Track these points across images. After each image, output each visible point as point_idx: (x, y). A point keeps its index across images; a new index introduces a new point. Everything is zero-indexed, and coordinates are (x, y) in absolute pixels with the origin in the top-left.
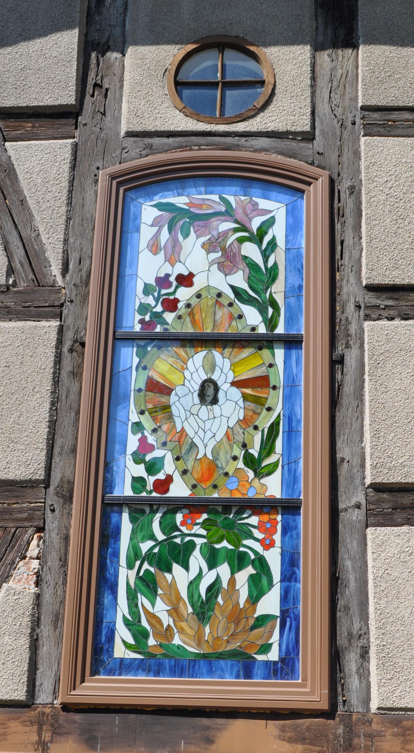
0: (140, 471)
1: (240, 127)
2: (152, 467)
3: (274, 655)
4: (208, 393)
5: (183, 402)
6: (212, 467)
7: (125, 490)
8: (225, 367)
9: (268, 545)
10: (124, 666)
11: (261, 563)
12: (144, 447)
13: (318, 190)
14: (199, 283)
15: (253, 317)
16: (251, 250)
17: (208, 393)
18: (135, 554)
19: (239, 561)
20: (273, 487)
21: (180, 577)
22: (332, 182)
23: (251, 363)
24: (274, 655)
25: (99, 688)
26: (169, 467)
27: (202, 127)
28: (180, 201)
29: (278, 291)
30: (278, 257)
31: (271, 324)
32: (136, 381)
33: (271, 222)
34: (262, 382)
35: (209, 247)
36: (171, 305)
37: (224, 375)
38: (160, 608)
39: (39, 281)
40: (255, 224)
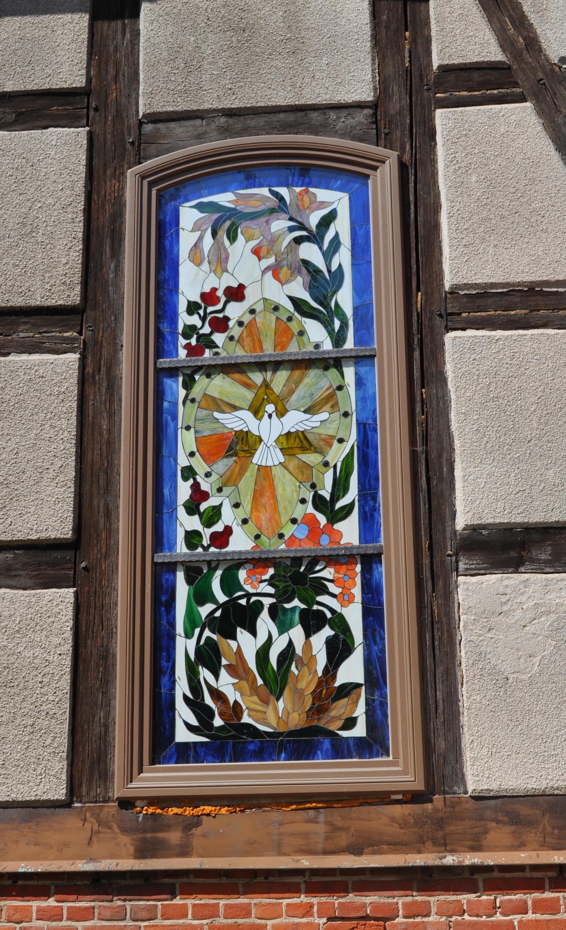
11: (339, 623)
19: (312, 622)
38: (225, 683)
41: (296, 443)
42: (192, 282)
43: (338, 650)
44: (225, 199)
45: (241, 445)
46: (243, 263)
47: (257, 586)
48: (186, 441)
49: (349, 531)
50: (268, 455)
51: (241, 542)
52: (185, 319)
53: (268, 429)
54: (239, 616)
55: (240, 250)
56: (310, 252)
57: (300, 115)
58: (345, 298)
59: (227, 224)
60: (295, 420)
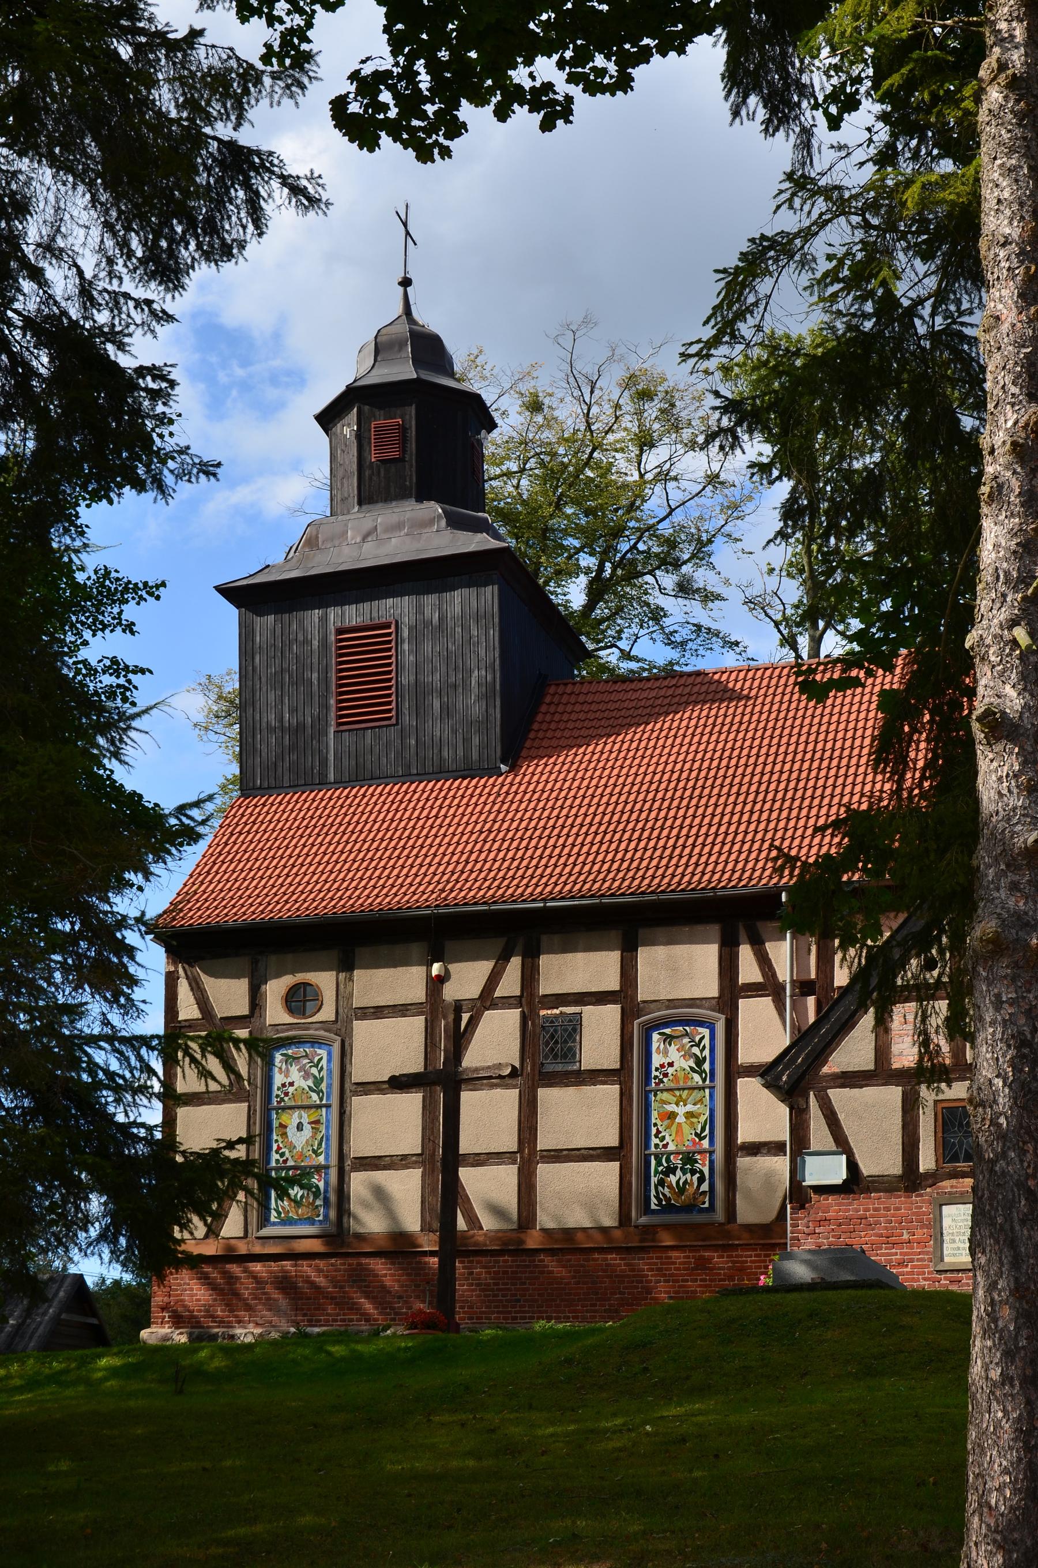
0: (277, 1157)
1: (310, 1020)
2: (282, 1155)
3: (707, 1205)
4: (300, 1127)
5: (291, 1131)
6: (301, 1154)
7: (273, 1164)
8: (306, 1117)
9: (704, 1165)
10: (274, 1224)
11: (701, 1172)
12: (279, 1148)
13: (336, 1048)
14: (296, 1085)
15: (315, 1097)
16: (314, 1071)
17: (300, 1127)
18: (656, 1172)
19: (693, 1172)
20: (321, 1159)
21: (673, 1179)
22: (343, 1042)
23: (314, 1115)
24: (707, 1205)
25: (266, 1232)
26: (287, 1154)
27: (296, 1021)
28: (290, 1052)
29: (323, 1086)
30: (324, 1073)
31: (321, 1099)
32: (275, 1124)
33: (320, 1060)
34: (317, 1122)
35: (299, 1070)
36: (286, 1094)
37: (305, 1120)
38: (666, 1191)
39: (242, 1088)
40: (697, 1039)
41: (689, 1115)
42: (657, 1060)
43: (701, 1180)
44: (668, 1031)
45: (672, 1116)
46: (674, 1054)
47: (677, 1161)
48: (654, 1115)
49: (705, 1144)
50: (680, 1119)
51: (671, 1147)
52: (654, 1073)
53: (681, 1110)
54: (671, 1170)
55: (673, 1049)
56: (696, 1050)
57: (692, 1002)
58: (706, 1066)
59: (668, 1039)
60: (689, 1108)
